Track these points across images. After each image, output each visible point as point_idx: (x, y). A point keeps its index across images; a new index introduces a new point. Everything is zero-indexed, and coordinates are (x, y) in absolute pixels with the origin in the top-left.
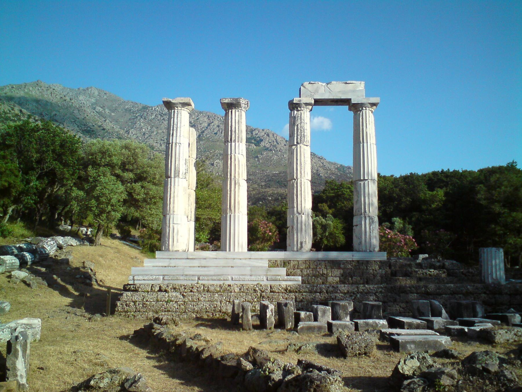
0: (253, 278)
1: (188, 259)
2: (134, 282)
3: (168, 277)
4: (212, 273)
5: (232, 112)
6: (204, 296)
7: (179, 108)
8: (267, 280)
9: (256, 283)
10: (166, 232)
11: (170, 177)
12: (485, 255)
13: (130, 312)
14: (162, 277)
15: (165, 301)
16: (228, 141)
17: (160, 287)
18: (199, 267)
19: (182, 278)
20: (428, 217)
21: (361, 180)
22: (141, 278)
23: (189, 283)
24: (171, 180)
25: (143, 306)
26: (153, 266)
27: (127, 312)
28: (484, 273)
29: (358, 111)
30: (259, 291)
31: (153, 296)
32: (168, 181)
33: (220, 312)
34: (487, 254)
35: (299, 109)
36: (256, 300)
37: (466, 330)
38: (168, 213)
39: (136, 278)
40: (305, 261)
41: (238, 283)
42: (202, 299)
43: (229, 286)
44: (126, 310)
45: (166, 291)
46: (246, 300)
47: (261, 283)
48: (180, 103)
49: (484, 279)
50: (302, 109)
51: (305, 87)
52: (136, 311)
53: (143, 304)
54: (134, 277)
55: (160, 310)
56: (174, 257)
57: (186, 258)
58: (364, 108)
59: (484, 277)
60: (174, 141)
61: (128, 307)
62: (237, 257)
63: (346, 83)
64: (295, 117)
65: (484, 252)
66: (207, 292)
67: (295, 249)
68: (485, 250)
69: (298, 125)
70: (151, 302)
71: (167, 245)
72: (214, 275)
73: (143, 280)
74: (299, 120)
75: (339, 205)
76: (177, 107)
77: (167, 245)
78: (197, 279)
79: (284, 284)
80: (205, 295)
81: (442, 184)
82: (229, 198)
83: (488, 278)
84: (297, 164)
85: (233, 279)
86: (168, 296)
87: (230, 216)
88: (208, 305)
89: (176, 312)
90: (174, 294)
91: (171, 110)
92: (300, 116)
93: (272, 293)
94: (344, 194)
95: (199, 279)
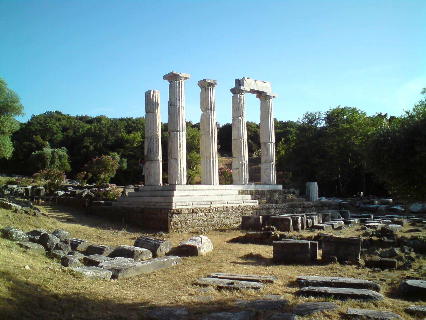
0: (237, 202)
1: (194, 190)
2: (176, 207)
3: (195, 203)
4: (217, 199)
5: (210, 89)
6: (216, 215)
7: (182, 81)
8: (243, 203)
9: (238, 205)
10: (178, 170)
11: (180, 131)
12: (312, 186)
13: (179, 229)
14: (191, 203)
15: (197, 220)
16: (209, 109)
17: (193, 210)
18: (205, 195)
19: (203, 203)
20: (130, 152)
21: (270, 142)
22: (180, 204)
23: (206, 206)
24: (180, 133)
25: (186, 224)
26: (180, 196)
27: (177, 229)
28: (311, 196)
29: (267, 100)
30: (241, 210)
31: (190, 217)
32: (177, 134)
33: (224, 224)
34: (313, 186)
35: (242, 94)
36: (240, 215)
37: (147, 234)
38: (179, 157)
39: (177, 204)
40: (244, 191)
41: (231, 205)
42: (215, 216)
43: (227, 207)
44: (176, 227)
45: (196, 213)
46: (235, 216)
47: (241, 205)
48: (184, 77)
49: (311, 199)
50: (244, 94)
51: (245, 80)
52: (182, 228)
53: (186, 223)
54: (176, 203)
55: (195, 226)
56: (186, 189)
57: (193, 189)
58: (270, 99)
59: (311, 198)
60: (181, 105)
61: (177, 226)
62: (233, 189)
63: (264, 82)
64: (240, 98)
65: (311, 185)
66: (217, 212)
67: (244, 184)
68: (312, 183)
69: (242, 104)
70: (190, 220)
71: (179, 180)
72: (218, 201)
73: (182, 206)
74: (243, 101)
75: (47, 137)
76: (181, 80)
77: (179, 180)
78: (210, 204)
79: (251, 204)
80: (216, 214)
81: (131, 128)
82: (211, 148)
83: (313, 198)
84: (243, 129)
85: (244, 202)
86: (199, 216)
87: (213, 161)
88: (218, 221)
89: (203, 226)
90: (202, 214)
91: (177, 81)
92: (243, 98)
93: (247, 211)
94: (52, 129)
95: (211, 203)
